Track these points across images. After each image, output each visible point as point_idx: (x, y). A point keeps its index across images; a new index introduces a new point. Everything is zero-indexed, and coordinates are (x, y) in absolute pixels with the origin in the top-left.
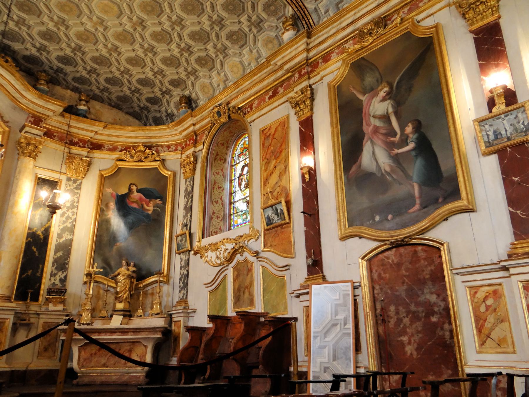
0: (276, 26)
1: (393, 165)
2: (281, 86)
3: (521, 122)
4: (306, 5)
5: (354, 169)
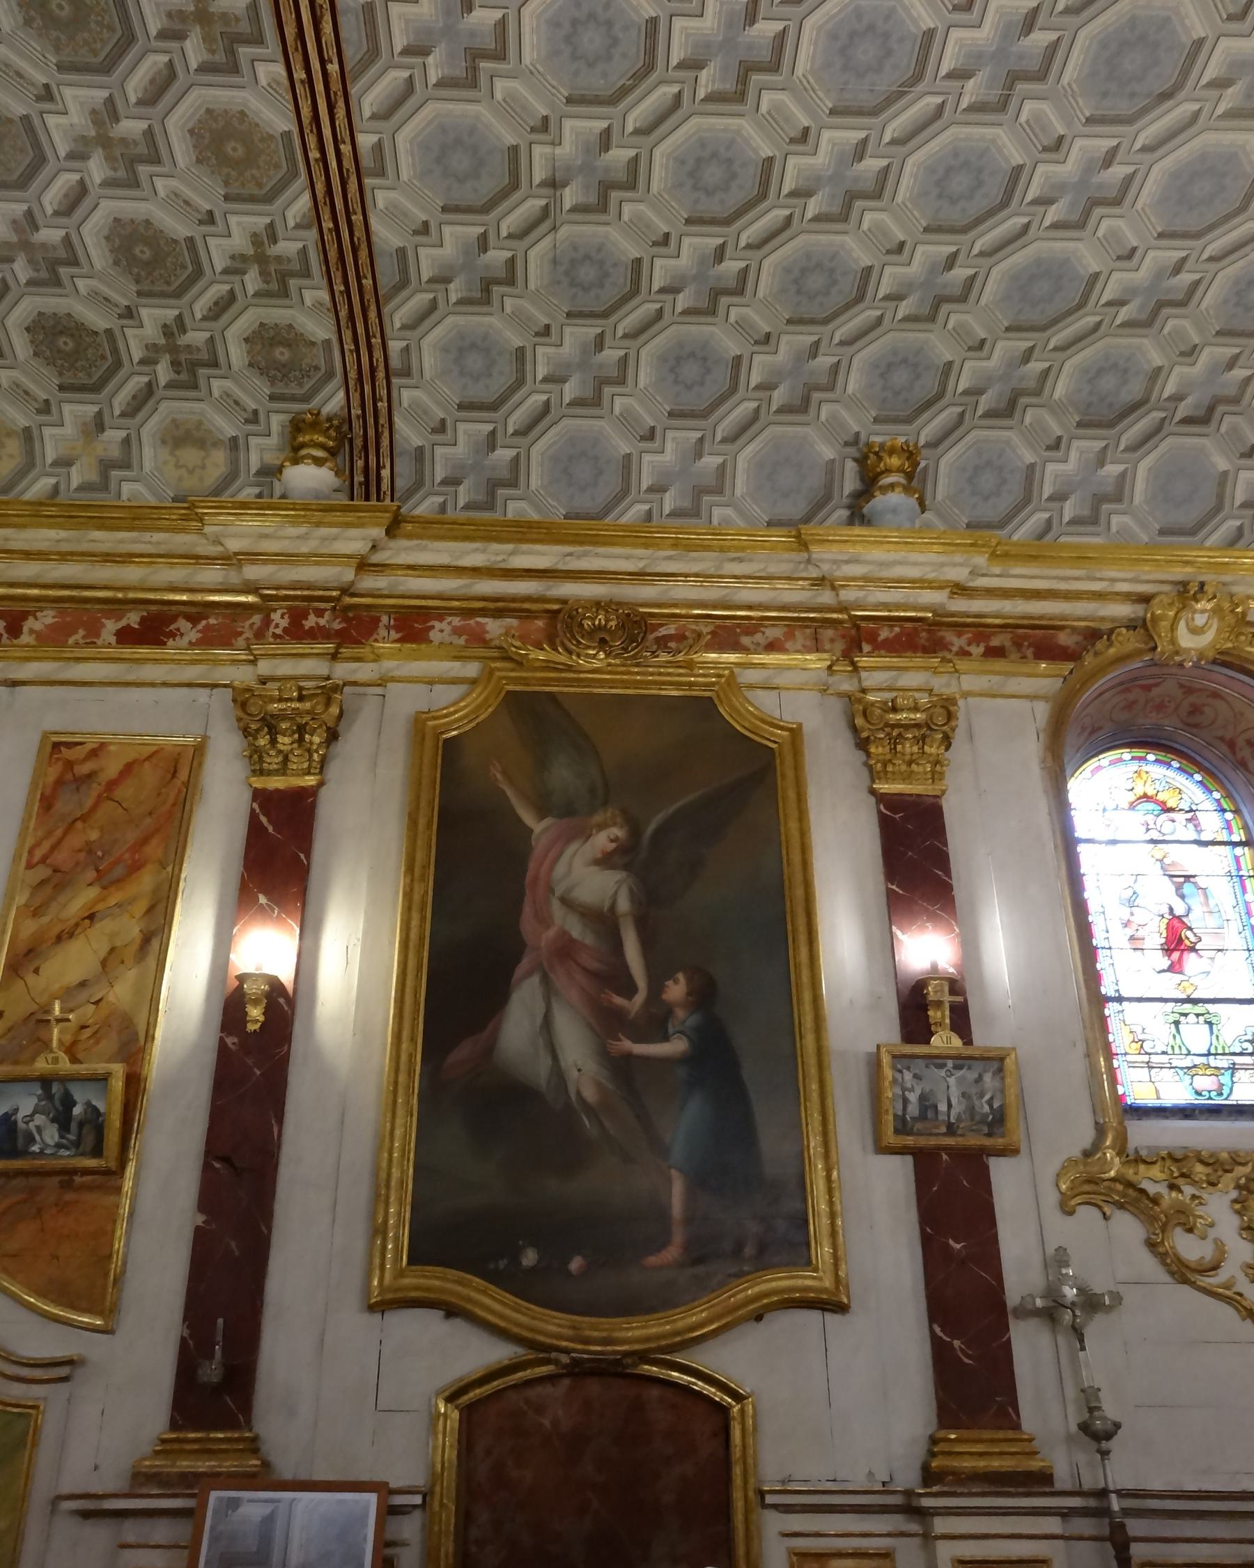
0: (255, 412)
1: (610, 1086)
2: (194, 619)
3: (987, 1097)
4: (397, 420)
5: (463, 1052)
